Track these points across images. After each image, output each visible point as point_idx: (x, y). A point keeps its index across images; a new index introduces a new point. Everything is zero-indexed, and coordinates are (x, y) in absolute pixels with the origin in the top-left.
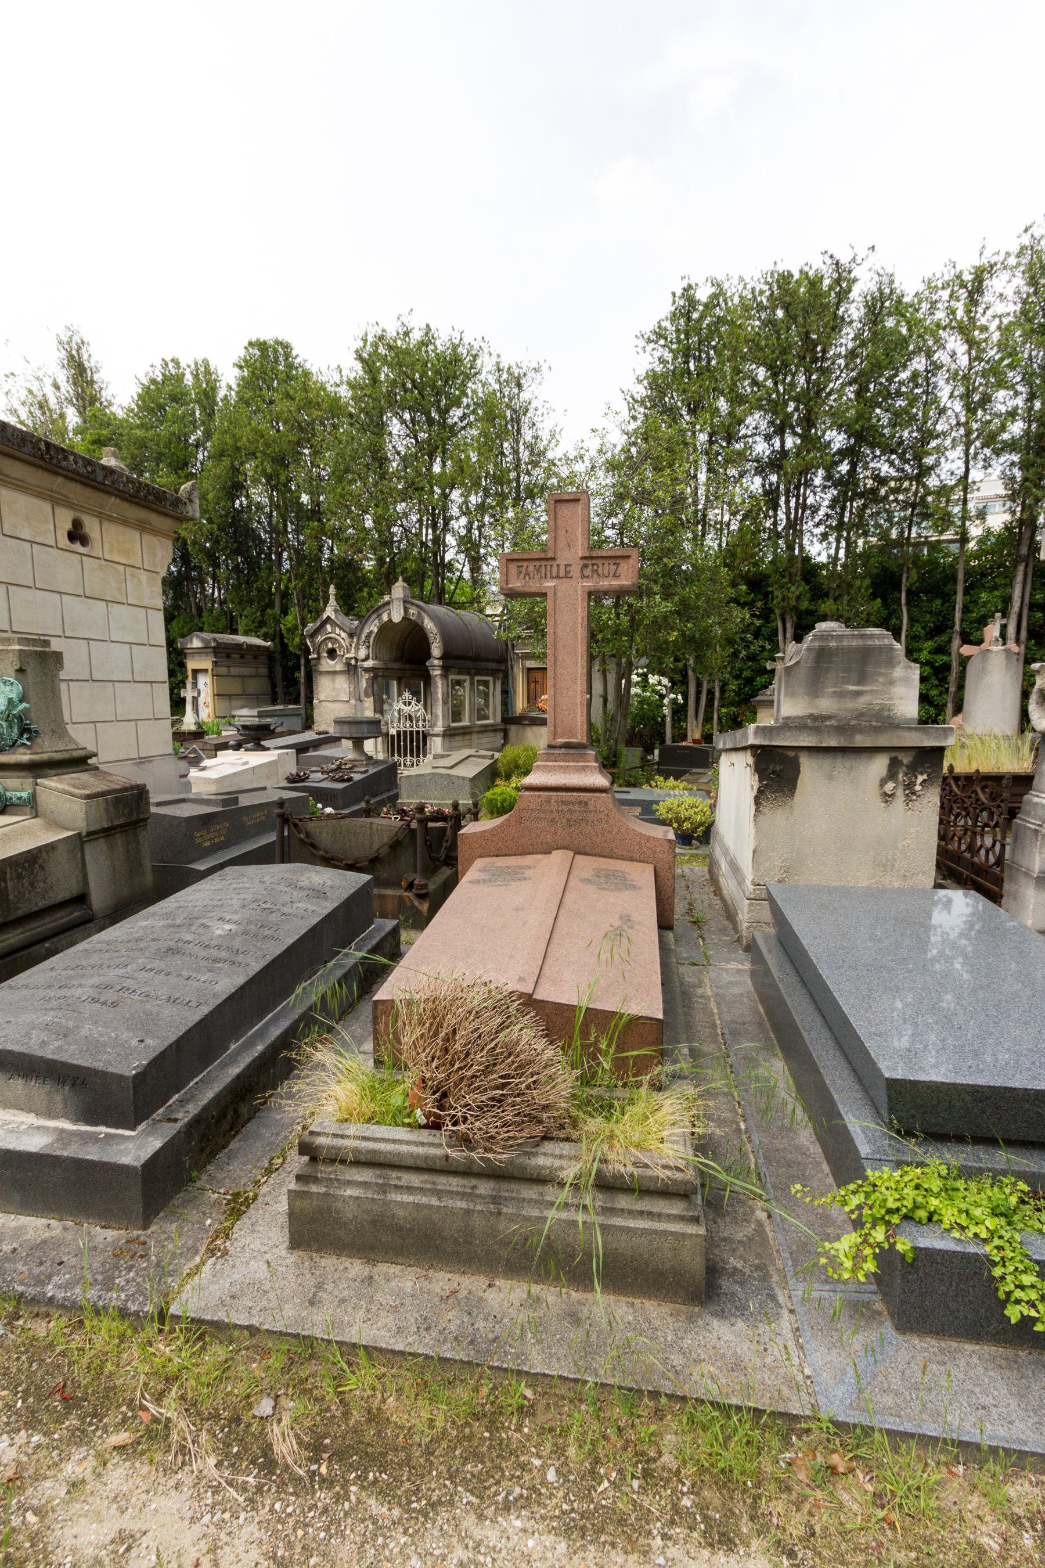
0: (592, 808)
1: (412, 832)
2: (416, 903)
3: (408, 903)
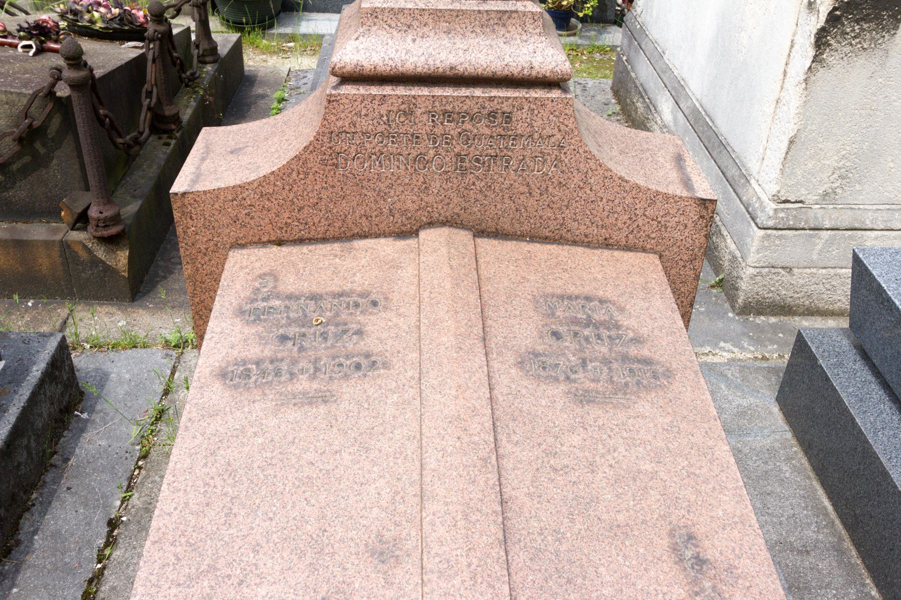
0: (521, 128)
1: (63, 105)
2: (101, 253)
3: (83, 255)
